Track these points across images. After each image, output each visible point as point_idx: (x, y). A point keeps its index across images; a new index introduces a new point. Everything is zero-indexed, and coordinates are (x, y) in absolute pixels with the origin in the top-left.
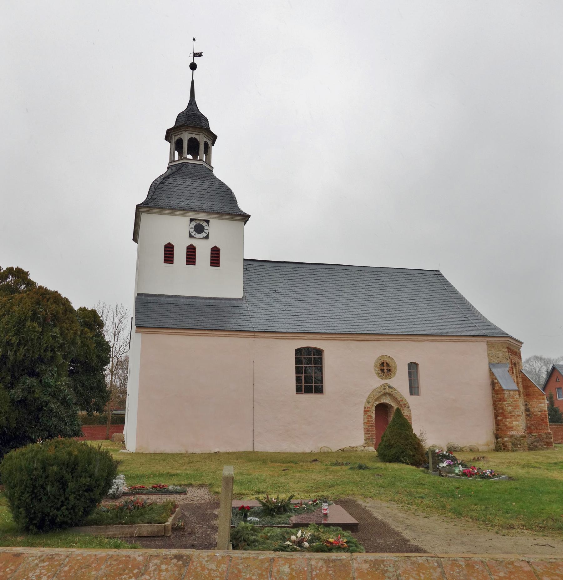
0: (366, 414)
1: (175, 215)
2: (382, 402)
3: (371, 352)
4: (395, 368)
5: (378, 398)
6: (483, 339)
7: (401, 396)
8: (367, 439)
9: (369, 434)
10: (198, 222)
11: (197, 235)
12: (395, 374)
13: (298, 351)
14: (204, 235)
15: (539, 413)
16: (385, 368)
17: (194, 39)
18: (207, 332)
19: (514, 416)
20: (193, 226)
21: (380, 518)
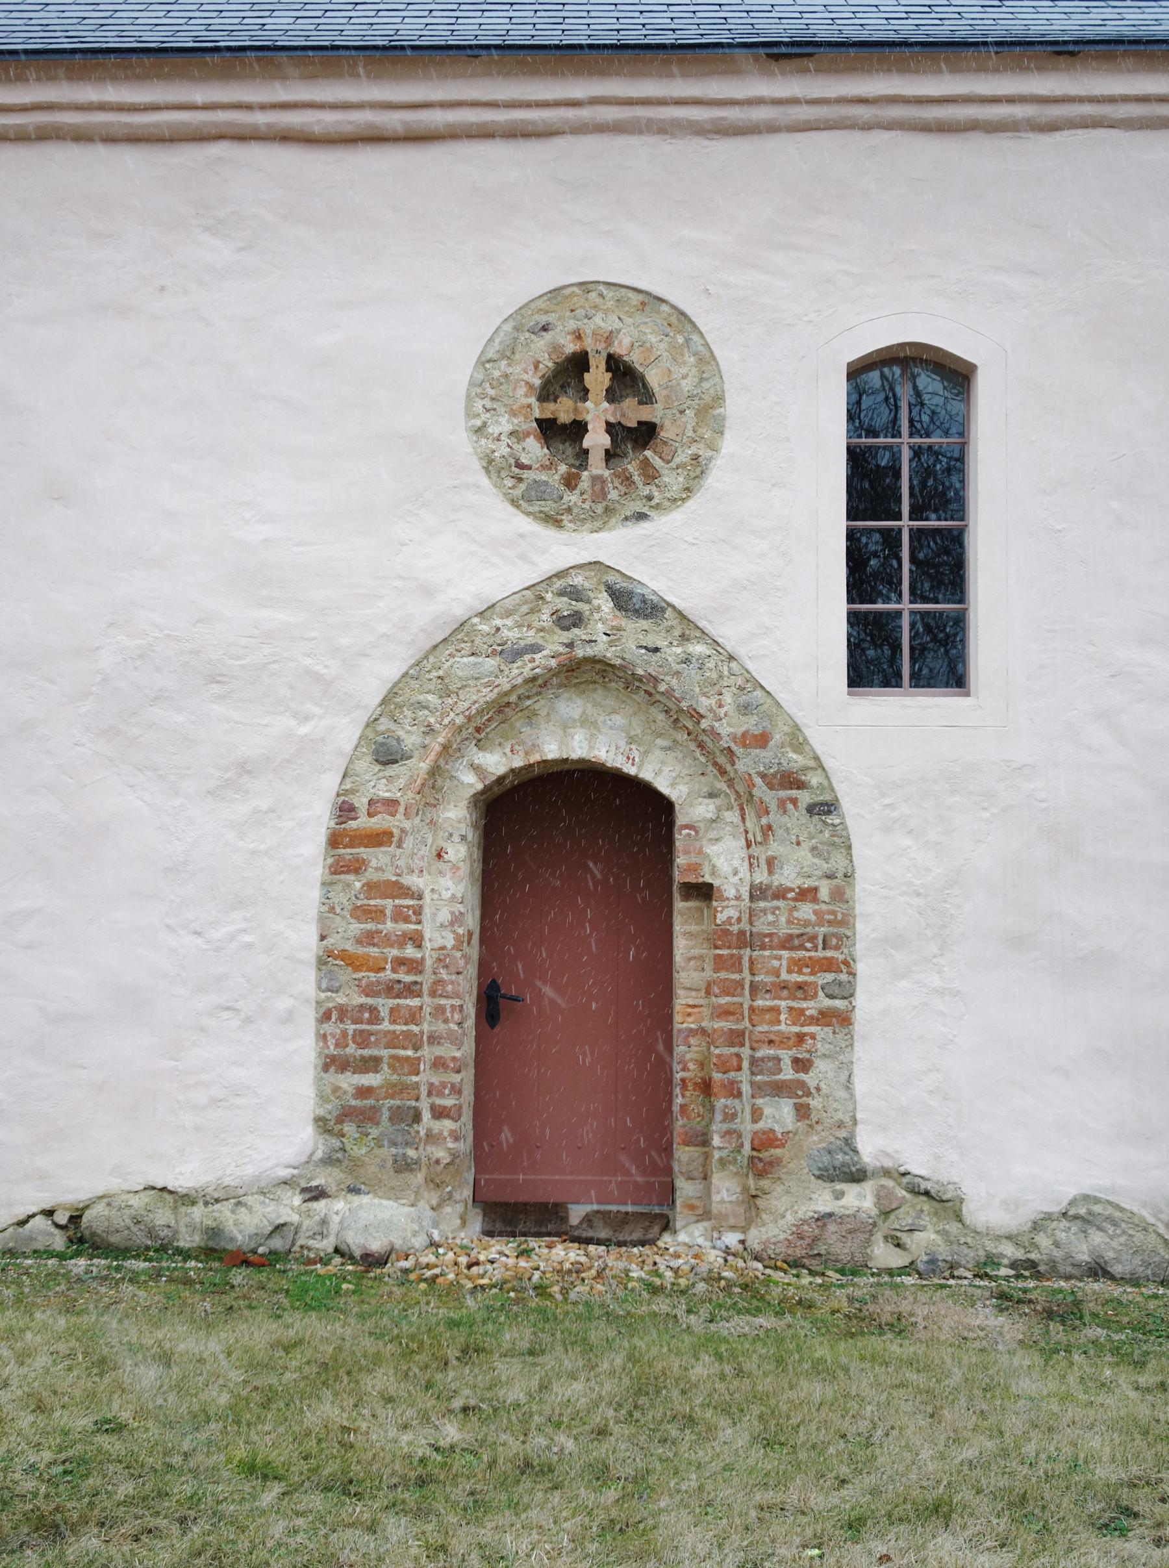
0: (356, 866)
2: (551, 750)
4: (709, 410)
5: (501, 714)
7: (752, 694)
8: (346, 1114)
9: (370, 1065)
12: (698, 468)
13: (795, 1104)
16: (597, 413)
21: (385, 1202)
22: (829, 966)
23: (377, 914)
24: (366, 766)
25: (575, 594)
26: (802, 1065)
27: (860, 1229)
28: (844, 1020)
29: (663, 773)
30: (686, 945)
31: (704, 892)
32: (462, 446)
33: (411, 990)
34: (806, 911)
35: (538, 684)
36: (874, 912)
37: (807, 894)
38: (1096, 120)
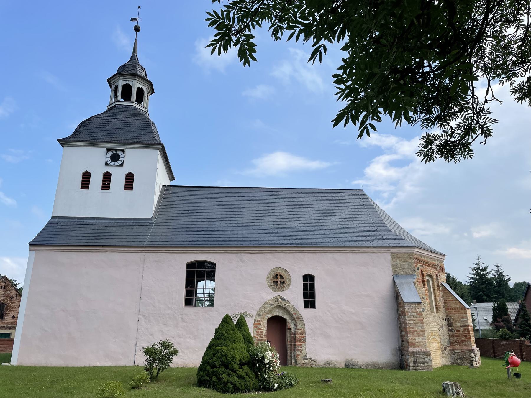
0: (256, 327)
1: (93, 146)
2: (275, 315)
3: (262, 265)
5: (270, 311)
6: (386, 249)
7: (295, 309)
10: (114, 152)
11: (112, 163)
12: (289, 286)
14: (119, 162)
15: (462, 329)
16: (279, 280)
17: (139, 7)
18: (355, 249)
19: (416, 331)
20: (110, 156)
22: (303, 337)
23: (258, 332)
24: (257, 317)
25: (277, 299)
26: (301, 347)
27: (307, 364)
28: (304, 343)
29: (286, 317)
30: (288, 335)
31: (290, 329)
32: (266, 284)
33: (262, 340)
34: (301, 331)
35: (274, 308)
36: (308, 331)
37: (301, 329)
38: (326, 252)
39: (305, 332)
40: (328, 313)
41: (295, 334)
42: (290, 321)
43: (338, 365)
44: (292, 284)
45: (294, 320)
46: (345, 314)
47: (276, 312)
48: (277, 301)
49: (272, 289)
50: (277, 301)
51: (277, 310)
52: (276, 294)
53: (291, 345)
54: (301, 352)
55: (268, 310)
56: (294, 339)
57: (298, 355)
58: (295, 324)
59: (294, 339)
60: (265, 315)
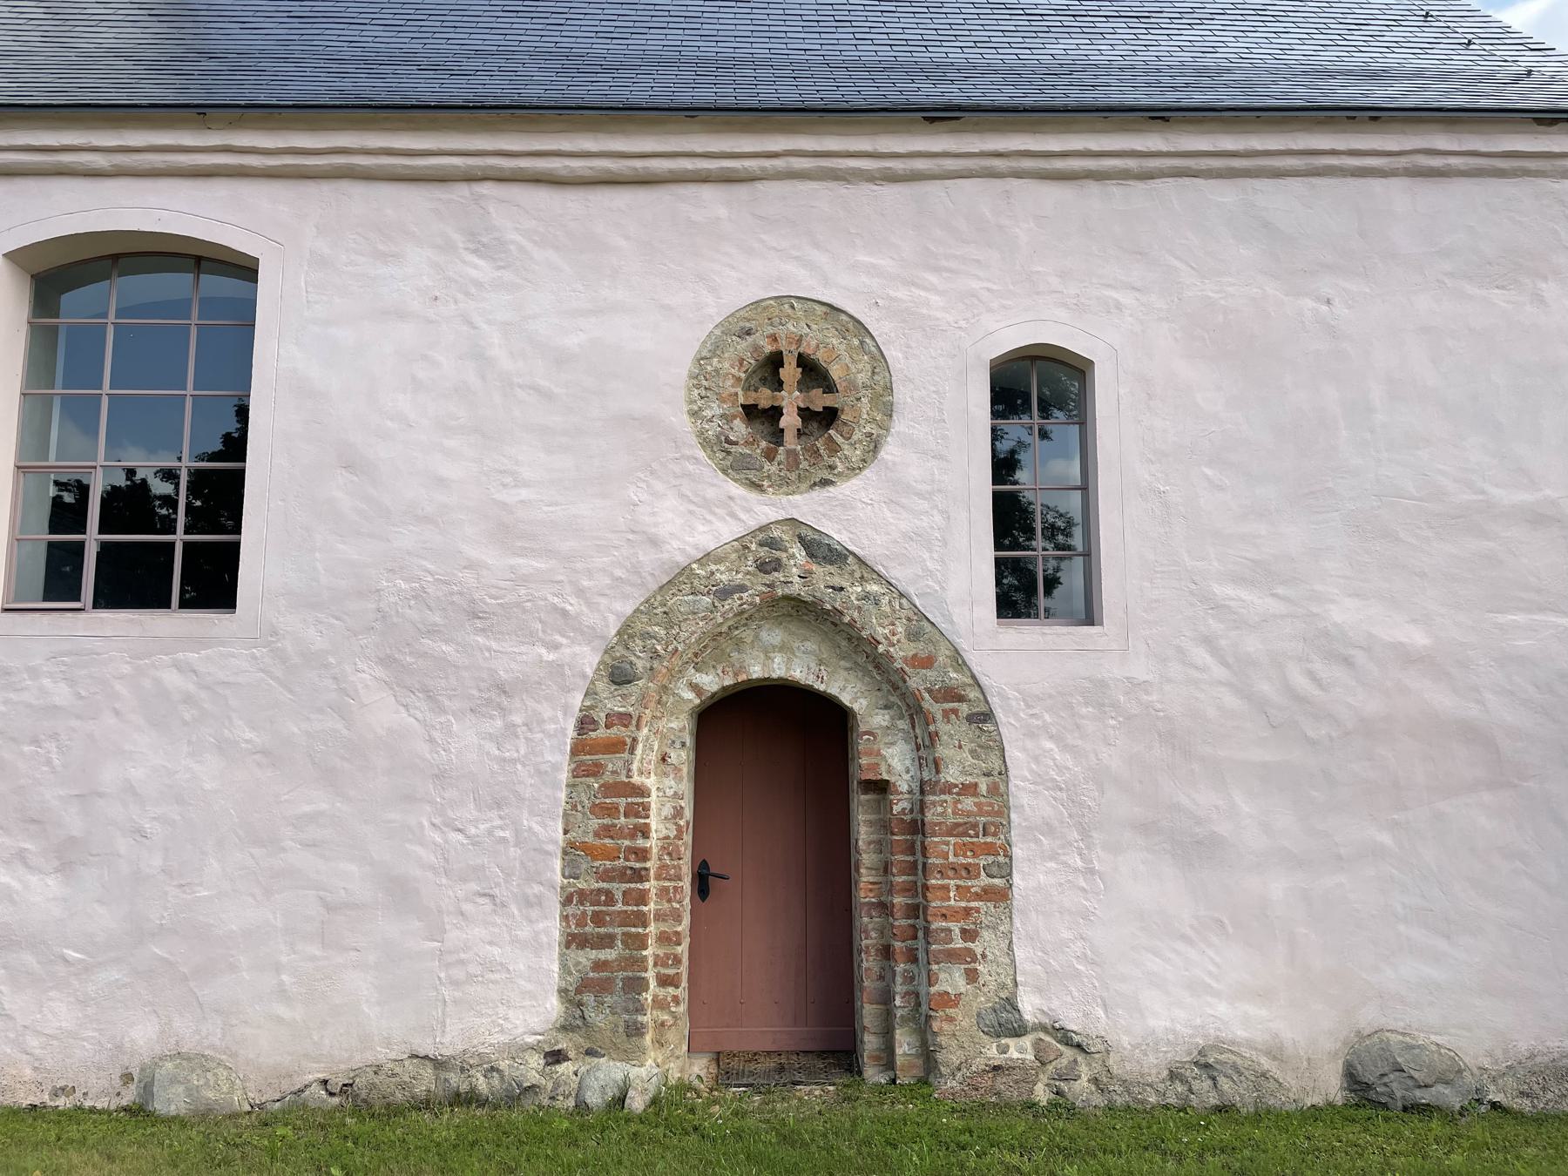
0: (595, 770)
2: (756, 671)
5: (715, 646)
7: (919, 625)
8: (585, 985)
9: (606, 941)
12: (874, 445)
16: (791, 400)
22: (990, 850)
23: (612, 811)
25: (772, 544)
27: (1026, 1076)
28: (1000, 896)
29: (847, 689)
30: (863, 832)
31: (881, 788)
32: (683, 424)
34: (968, 803)
35: (745, 618)
36: (1027, 800)
37: (970, 789)
39: (1003, 810)
40: (1201, 655)
41: (917, 827)
42: (880, 719)
43: (1290, 1080)
44: (899, 425)
45: (913, 711)
46: (1347, 662)
47: (767, 652)
48: (777, 565)
49: (737, 467)
50: (777, 565)
51: (773, 635)
52: (765, 509)
53: (884, 908)
54: (972, 976)
55: (692, 631)
56: (912, 868)
57: (948, 1000)
58: (925, 748)
59: (912, 868)
60: (674, 675)
